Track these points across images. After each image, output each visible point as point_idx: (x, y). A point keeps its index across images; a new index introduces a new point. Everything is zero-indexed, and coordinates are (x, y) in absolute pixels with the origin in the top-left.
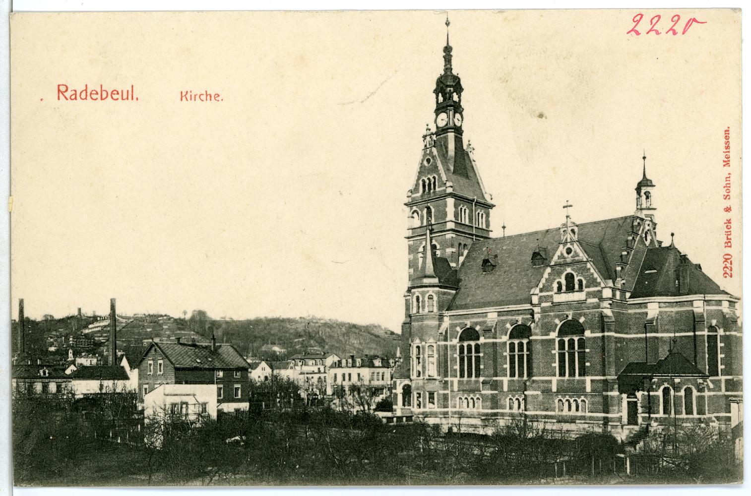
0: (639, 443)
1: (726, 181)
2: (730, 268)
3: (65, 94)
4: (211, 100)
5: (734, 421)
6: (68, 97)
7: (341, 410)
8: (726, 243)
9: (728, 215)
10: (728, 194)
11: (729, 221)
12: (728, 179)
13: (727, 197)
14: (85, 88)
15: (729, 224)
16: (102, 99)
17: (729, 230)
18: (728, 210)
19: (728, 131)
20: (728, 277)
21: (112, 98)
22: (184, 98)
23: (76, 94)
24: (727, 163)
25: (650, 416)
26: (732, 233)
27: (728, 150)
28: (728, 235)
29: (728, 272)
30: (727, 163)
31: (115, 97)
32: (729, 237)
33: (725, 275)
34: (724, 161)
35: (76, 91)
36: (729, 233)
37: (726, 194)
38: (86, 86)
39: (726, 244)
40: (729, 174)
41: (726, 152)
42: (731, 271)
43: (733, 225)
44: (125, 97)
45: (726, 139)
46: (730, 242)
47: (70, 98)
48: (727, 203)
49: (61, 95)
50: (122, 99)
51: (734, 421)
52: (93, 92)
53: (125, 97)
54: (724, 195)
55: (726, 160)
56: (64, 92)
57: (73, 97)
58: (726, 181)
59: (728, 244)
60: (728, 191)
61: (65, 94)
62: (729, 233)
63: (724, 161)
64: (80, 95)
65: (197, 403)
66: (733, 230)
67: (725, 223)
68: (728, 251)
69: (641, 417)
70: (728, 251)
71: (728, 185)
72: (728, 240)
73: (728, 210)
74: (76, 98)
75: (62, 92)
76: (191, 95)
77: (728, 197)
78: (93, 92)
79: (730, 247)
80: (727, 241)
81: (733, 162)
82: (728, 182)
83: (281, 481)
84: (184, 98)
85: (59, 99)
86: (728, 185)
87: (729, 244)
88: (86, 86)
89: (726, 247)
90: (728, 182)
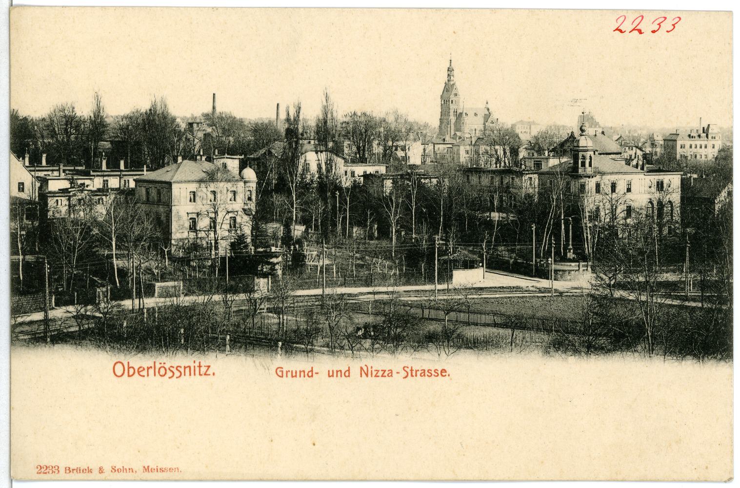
1: (130, 469)
2: (46, 471)
4: (300, 376)
7: (229, 296)
8: (69, 468)
12: (90, 471)
14: (348, 369)
15: (87, 471)
16: (129, 376)
17: (81, 471)
19: (132, 471)
20: (37, 470)
21: (441, 375)
25: (245, 155)
27: (159, 470)
29: (43, 470)
31: (444, 374)
32: (75, 471)
33: (39, 467)
34: (148, 467)
35: (391, 370)
36: (78, 471)
37: (116, 469)
38: (312, 368)
39: (68, 469)
42: (44, 473)
43: (130, 475)
45: (118, 470)
46: (70, 471)
52: (140, 370)
55: (150, 469)
58: (130, 469)
59: (69, 470)
60: (119, 470)
62: (78, 471)
63: (148, 467)
64: (134, 371)
66: (81, 476)
69: (134, 180)
71: (125, 471)
73: (101, 470)
77: (113, 471)
78: (140, 370)
80: (71, 470)
81: (68, 476)
82: (128, 470)
85: (361, 376)
87: (68, 471)
88: (312, 368)
90: (128, 470)
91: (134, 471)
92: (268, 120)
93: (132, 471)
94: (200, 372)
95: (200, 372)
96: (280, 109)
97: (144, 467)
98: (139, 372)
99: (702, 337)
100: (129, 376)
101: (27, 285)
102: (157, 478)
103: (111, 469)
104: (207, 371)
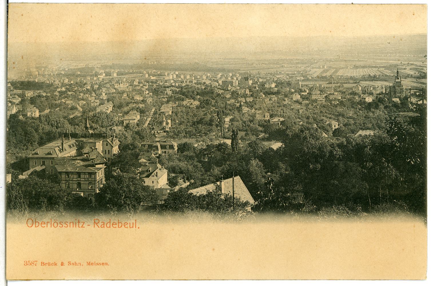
0: (26, 157)
3: (98, 224)
5: (166, 175)
6: (100, 226)
9: (59, 264)
10: (71, 264)
11: (56, 264)
13: (69, 263)
18: (62, 264)
19: (107, 265)
22: (52, 226)
23: (104, 224)
24: (89, 264)
26: (49, 266)
27: (96, 264)
28: (48, 264)
30: (89, 264)
32: (47, 265)
34: (90, 263)
36: (49, 265)
37: (71, 263)
39: (43, 263)
40: (109, 265)
41: (95, 264)
44: (131, 226)
47: (101, 227)
48: (66, 263)
49: (96, 225)
50: (119, 227)
51: (166, 175)
53: (131, 226)
54: (71, 262)
55: (91, 263)
56: (98, 223)
57: (103, 226)
61: (98, 224)
63: (90, 263)
65: (95, 223)
67: (55, 263)
68: (39, 264)
70: (39, 264)
71: (76, 264)
72: (45, 264)
73: (62, 264)
74: (104, 227)
75: (96, 223)
76: (136, 228)
77: (69, 264)
79: (42, 265)
82: (78, 264)
83: (383, 211)
84: (52, 226)
86: (76, 264)
87: (43, 265)
89: (42, 262)
91: (108, 265)
92: (40, 214)
93: (107, 265)
94: (130, 226)
95: (130, 226)
96: (135, 227)
97: (87, 262)
98: (124, 226)
99: (418, 208)
100: (36, 227)
101: (12, 204)
102: (135, 225)
103: (68, 263)
104: (82, 225)
